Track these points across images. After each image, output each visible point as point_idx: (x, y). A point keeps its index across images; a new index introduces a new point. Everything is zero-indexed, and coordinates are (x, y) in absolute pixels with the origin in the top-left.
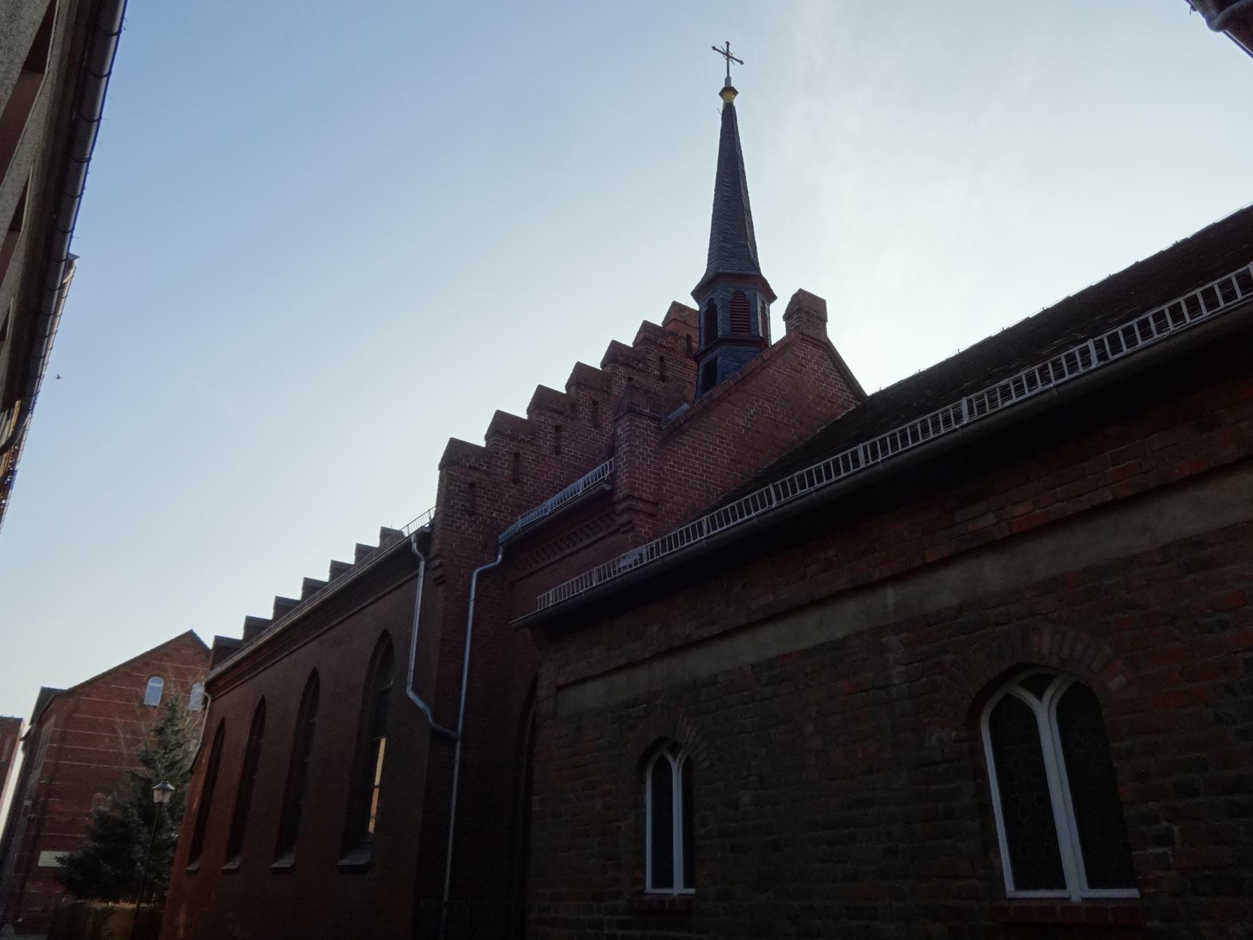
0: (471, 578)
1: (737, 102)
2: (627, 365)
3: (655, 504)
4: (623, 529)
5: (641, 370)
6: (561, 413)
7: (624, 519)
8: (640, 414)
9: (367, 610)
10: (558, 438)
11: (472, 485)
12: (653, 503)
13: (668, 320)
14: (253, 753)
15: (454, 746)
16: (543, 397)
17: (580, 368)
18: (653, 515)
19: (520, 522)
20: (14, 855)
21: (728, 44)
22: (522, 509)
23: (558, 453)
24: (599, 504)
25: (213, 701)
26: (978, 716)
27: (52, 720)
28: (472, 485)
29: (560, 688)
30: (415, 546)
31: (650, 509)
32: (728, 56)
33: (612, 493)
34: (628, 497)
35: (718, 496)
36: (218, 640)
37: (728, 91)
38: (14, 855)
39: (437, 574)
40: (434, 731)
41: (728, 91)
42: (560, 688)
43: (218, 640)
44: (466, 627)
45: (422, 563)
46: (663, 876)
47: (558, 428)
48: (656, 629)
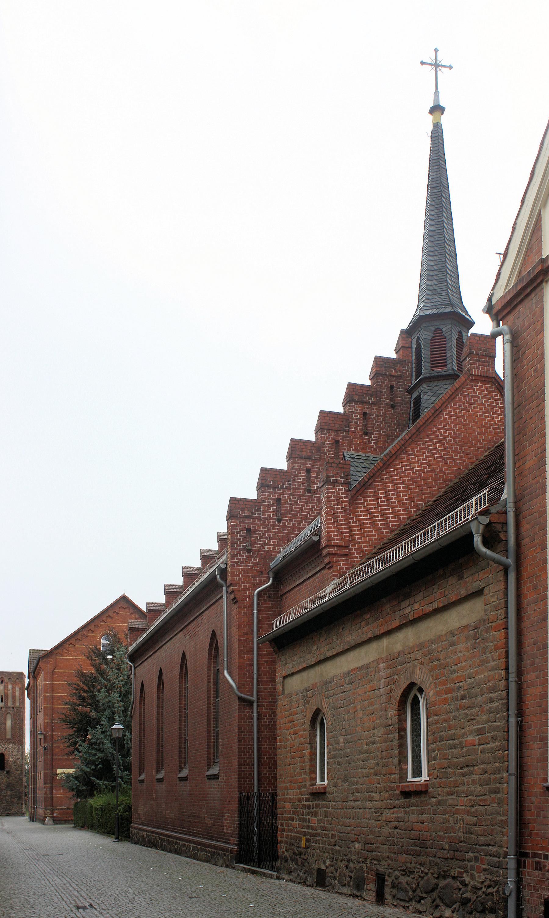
0: (253, 597)
1: (445, 120)
2: (361, 402)
3: (346, 547)
4: (328, 567)
5: (374, 404)
6: (309, 458)
7: (326, 560)
8: (334, 483)
9: (189, 627)
10: (309, 478)
11: (249, 530)
12: (345, 547)
13: (375, 376)
14: (184, 694)
15: (252, 705)
16: (297, 448)
17: (324, 415)
18: (345, 555)
19: (280, 556)
20: (41, 773)
21: (436, 50)
22: (286, 540)
23: (309, 491)
24: (312, 551)
25: (135, 668)
26: (406, 703)
27: (42, 675)
28: (249, 530)
29: (285, 677)
30: (218, 577)
31: (343, 551)
32: (436, 65)
33: (319, 542)
34: (328, 546)
35: (395, 530)
36: (148, 605)
37: (437, 109)
38: (41, 773)
39: (232, 596)
40: (240, 698)
41: (437, 109)
42: (285, 677)
43: (148, 605)
44: (253, 630)
45: (225, 588)
46: (417, 772)
47: (308, 471)
48: (315, 648)
